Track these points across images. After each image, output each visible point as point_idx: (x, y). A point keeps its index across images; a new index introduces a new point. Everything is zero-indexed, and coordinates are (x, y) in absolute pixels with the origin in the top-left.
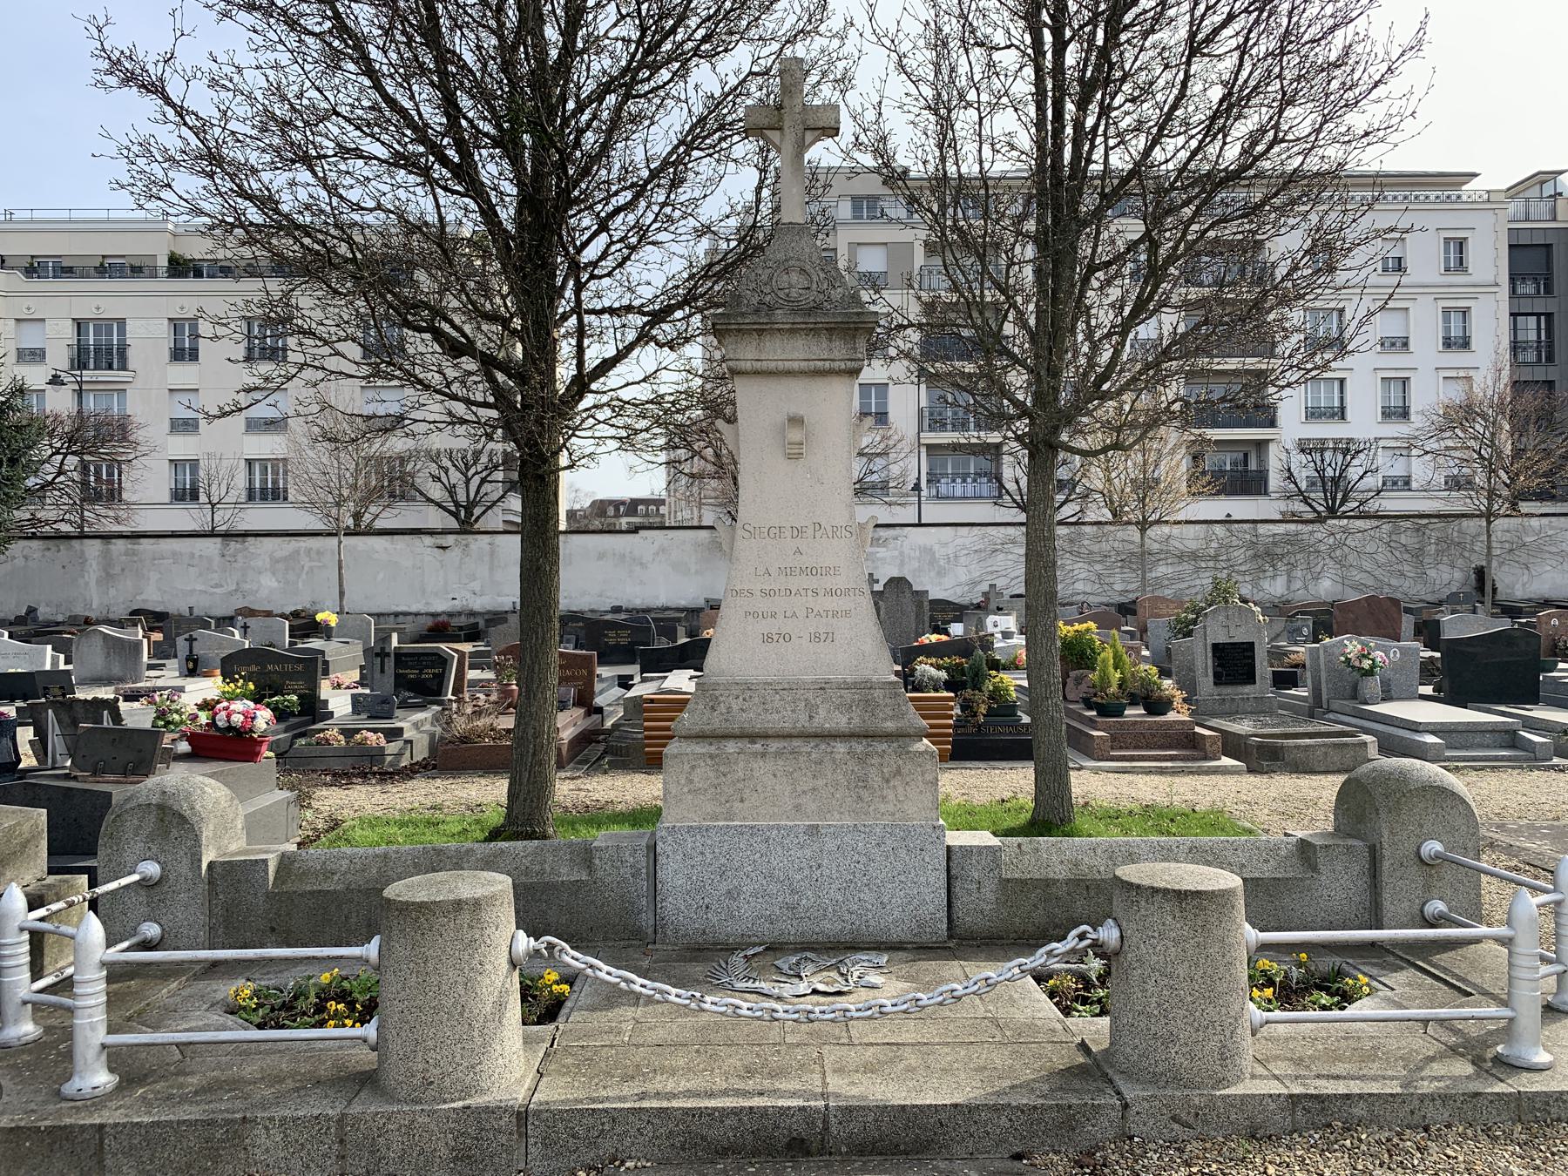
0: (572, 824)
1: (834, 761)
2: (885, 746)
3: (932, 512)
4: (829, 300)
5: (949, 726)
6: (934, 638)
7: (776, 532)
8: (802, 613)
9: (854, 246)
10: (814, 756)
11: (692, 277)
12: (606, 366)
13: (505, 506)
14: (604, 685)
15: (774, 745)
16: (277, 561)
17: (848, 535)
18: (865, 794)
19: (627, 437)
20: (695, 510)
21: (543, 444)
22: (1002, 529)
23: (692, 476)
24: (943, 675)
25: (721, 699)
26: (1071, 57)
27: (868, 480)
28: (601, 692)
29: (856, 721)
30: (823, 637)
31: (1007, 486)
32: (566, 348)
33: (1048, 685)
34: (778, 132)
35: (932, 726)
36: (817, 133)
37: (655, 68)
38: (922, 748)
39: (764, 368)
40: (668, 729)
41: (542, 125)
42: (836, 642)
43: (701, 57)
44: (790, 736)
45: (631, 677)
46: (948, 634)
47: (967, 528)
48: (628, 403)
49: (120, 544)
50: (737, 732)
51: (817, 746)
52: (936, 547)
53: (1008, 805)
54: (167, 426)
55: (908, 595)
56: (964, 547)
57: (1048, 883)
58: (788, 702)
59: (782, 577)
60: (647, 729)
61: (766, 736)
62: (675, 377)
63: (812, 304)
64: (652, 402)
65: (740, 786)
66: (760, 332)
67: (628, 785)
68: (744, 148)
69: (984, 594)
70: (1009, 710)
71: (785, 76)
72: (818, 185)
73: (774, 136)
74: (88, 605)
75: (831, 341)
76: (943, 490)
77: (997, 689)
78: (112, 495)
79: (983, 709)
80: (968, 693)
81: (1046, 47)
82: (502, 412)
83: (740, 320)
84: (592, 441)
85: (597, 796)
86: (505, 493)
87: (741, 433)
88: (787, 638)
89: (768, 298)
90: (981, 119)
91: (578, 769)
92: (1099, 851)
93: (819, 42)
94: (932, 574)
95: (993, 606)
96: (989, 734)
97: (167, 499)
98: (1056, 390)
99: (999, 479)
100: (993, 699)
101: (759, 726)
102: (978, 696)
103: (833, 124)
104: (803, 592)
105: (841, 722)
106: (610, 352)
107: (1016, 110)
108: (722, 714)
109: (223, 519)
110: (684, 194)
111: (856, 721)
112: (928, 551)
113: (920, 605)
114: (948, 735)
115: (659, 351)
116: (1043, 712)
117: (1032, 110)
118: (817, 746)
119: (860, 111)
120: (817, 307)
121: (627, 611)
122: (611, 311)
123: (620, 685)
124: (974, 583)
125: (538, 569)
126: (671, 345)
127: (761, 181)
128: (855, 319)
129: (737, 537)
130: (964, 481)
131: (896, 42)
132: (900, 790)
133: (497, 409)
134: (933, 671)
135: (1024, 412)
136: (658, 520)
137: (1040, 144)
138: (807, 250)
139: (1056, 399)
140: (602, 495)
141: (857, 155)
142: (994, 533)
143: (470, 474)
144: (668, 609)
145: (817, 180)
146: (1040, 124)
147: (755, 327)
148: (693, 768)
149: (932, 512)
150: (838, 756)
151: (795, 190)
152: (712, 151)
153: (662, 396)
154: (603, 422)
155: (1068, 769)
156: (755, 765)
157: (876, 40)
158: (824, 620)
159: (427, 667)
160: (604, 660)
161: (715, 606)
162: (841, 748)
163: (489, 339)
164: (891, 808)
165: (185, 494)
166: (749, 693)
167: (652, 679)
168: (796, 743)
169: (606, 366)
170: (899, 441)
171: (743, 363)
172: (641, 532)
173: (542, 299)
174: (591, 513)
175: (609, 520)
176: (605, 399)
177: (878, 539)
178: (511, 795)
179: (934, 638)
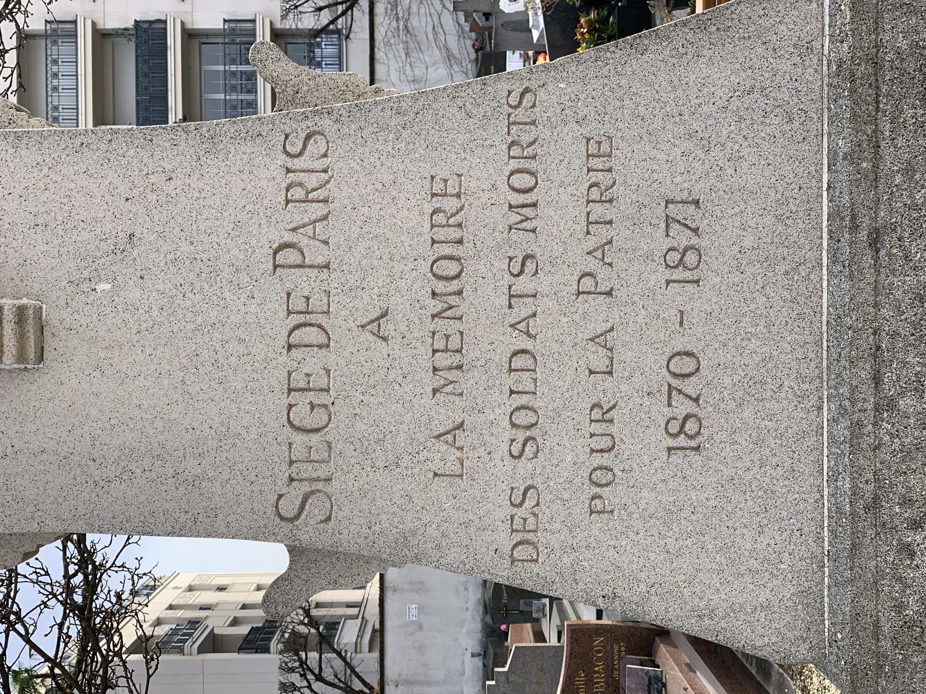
13: (351, 649)
17: (317, 146)
22: (378, 20)
30: (683, 238)
31: (325, 22)
42: (700, 189)
56: (402, 71)
59: (469, 381)
86: (335, 651)
99: (317, 33)
104: (523, 309)
142: (383, 31)
158: (620, 233)
166: (892, 509)
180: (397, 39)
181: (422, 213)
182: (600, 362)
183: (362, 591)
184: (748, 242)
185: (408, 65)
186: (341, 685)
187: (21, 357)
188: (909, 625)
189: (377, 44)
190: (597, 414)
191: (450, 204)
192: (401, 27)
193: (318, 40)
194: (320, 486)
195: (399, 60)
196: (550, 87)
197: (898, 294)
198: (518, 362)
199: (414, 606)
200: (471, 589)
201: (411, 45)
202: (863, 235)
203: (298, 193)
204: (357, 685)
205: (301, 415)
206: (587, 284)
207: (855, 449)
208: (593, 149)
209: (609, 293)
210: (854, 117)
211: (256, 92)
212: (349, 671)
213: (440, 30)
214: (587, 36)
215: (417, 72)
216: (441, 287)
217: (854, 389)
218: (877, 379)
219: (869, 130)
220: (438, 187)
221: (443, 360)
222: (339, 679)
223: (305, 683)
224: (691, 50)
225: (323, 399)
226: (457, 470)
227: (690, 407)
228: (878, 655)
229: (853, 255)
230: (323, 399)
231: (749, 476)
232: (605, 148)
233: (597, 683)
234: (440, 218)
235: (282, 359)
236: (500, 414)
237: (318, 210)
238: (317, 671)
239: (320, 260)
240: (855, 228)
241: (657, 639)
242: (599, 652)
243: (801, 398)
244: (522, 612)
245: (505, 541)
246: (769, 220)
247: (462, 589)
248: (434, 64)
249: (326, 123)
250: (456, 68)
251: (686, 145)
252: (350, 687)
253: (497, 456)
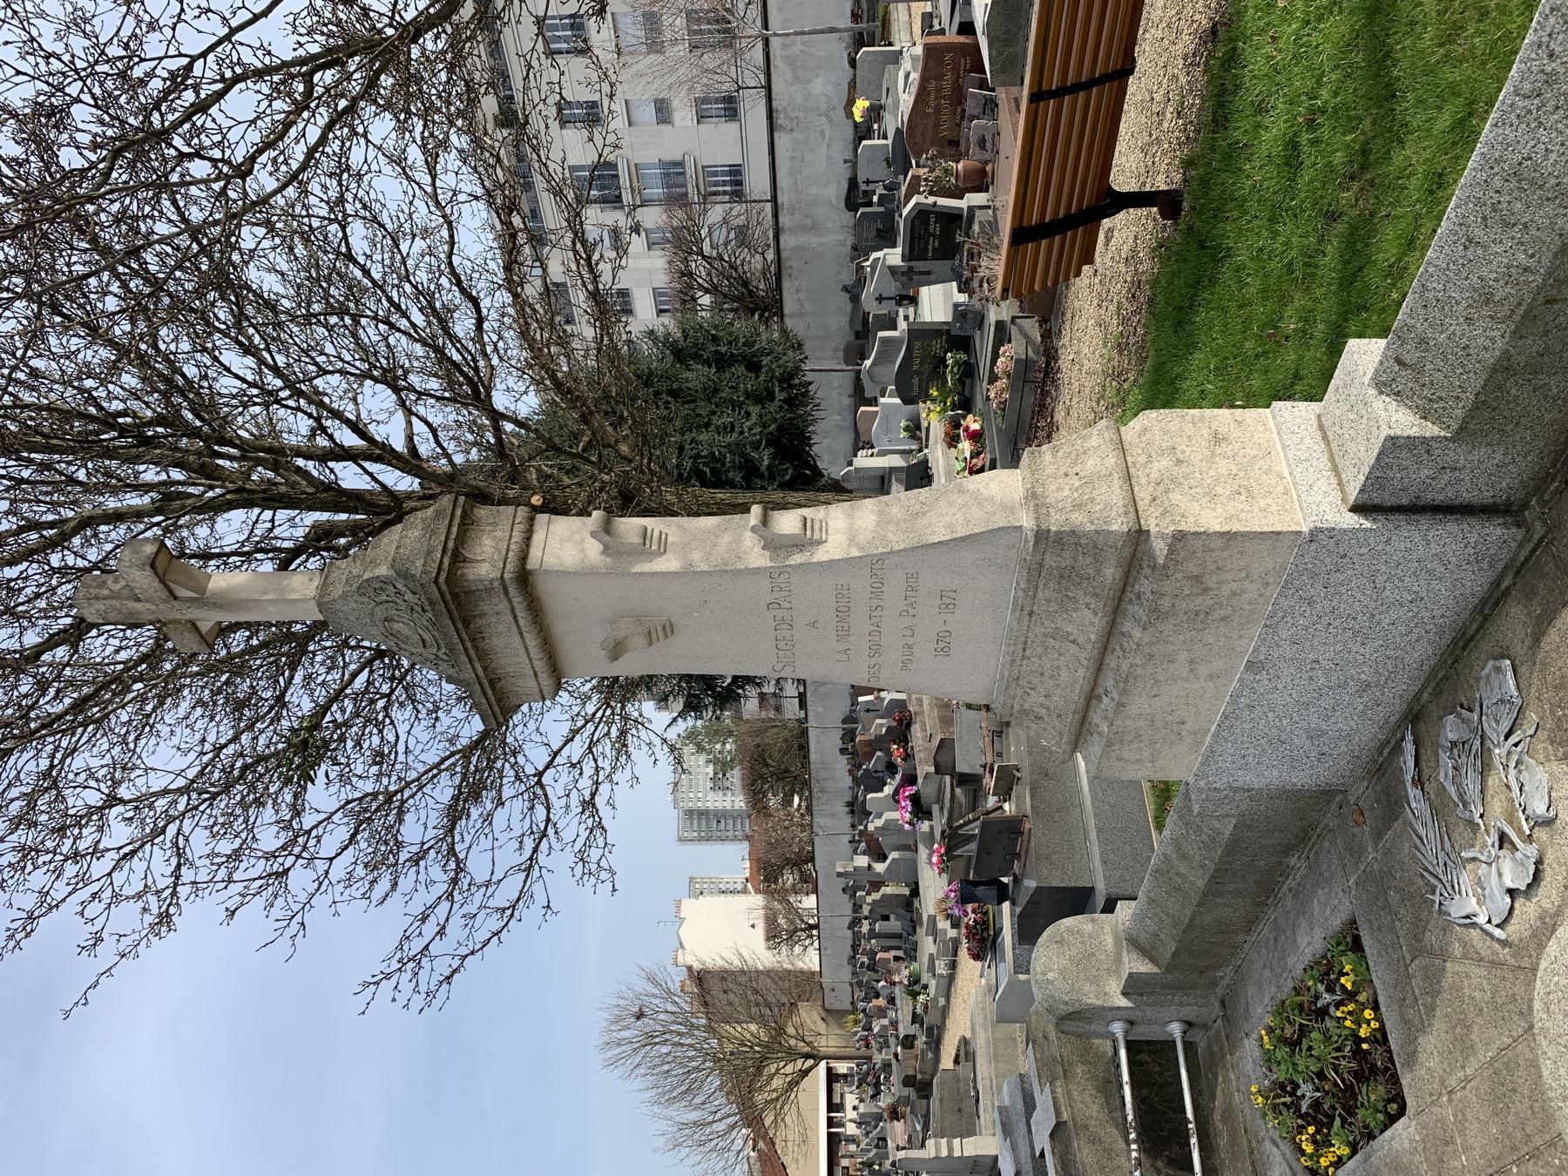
16: (797, 78)
49: (784, 220)
54: (664, 128)
57: (1503, 369)
74: (841, 243)
78: (736, 172)
92: (1478, 233)
97: (734, 126)
109: (752, 78)
147: (489, 692)
159: (927, 230)
165: (731, 108)
218: (1024, 650)
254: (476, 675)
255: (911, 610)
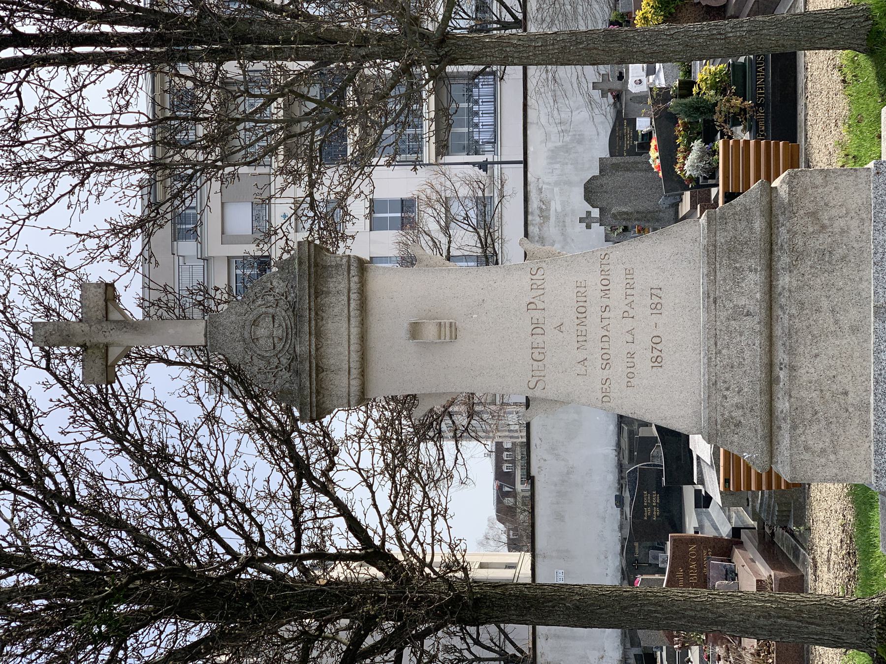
0: (869, 575)
1: (800, 288)
2: (783, 230)
3: (511, 149)
4: (285, 295)
5: (758, 145)
6: (654, 154)
7: (538, 354)
8: (629, 324)
9: (226, 238)
10: (794, 311)
11: (259, 431)
12: (355, 527)
14: (707, 524)
15: (781, 356)
17: (540, 272)
18: (839, 252)
19: (432, 508)
20: (509, 409)
21: (441, 599)
23: (470, 416)
24: (697, 145)
25: (727, 415)
26: (29, 28)
27: (474, 221)
28: (716, 529)
29: (752, 262)
30: (656, 300)
32: (339, 571)
33: (711, 37)
34: (111, 349)
35: (757, 178)
36: (111, 307)
37: (43, 472)
38: (785, 187)
39: (357, 365)
40: (759, 476)
41: (104, 598)
43: (31, 425)
44: (770, 338)
45: (698, 492)
46: (648, 136)
47: (530, 111)
48: (394, 503)
50: (765, 398)
51: (782, 307)
52: (550, 145)
53: (849, 77)
55: (604, 180)
56: (550, 115)
58: (731, 338)
60: (759, 487)
61: (770, 366)
62: (366, 455)
63: (290, 313)
64: (393, 477)
65: (828, 395)
66: (319, 369)
67: (824, 505)
68: (126, 378)
69: (604, 95)
70: (738, 74)
71: (51, 341)
72: (164, 299)
73: (114, 352)
75: (328, 293)
76: (485, 136)
77: (714, 86)
79: (737, 102)
80: (718, 118)
81: (20, 54)
82: (406, 643)
83: (307, 392)
84: (437, 547)
85: (836, 542)
87: (428, 391)
88: (656, 341)
89: (284, 361)
90: (94, 127)
91: (805, 560)
93: (14, 296)
94: (580, 149)
95: (617, 85)
96: (766, 93)
98: (382, 37)
100: (725, 90)
101: (759, 374)
102: (722, 107)
103: (101, 290)
104: (605, 322)
105: (754, 280)
106: (341, 523)
107: (84, 86)
108: (744, 415)
110: (174, 443)
111: (752, 262)
112: (554, 155)
113: (616, 167)
114: (768, 145)
115: (339, 467)
116: (742, 42)
117: (84, 68)
118: (782, 307)
119: (85, 253)
120: (293, 307)
121: (621, 488)
122: (297, 523)
123: (707, 506)
124: (591, 102)
125: (577, 608)
126: (332, 454)
127: (161, 360)
128: (305, 267)
129: (543, 396)
130: (476, 114)
131: (15, 219)
132: (834, 212)
133: (403, 649)
134: (693, 156)
135: (405, 70)
136: (518, 449)
137: (118, 61)
138: (233, 318)
139: (391, 36)
140: (492, 512)
141: (132, 256)
142: (534, 81)
143: (470, 657)
144: (618, 445)
145: (160, 300)
146: (96, 60)
148: (807, 448)
149: (511, 149)
150: (795, 284)
151: (171, 331)
152: (128, 410)
153: (387, 465)
154: (416, 531)
155: (806, 14)
156: (805, 378)
157: (12, 241)
160: (677, 525)
161: (622, 420)
162: (784, 281)
163: (327, 649)
164: (854, 223)
166: (720, 384)
167: (700, 472)
168: (778, 331)
169: (355, 527)
170: (432, 187)
171: (353, 389)
172: (532, 474)
173: (285, 596)
174: (511, 522)
175: (519, 504)
176: (391, 531)
177: (541, 209)
178: (835, 643)
179: (654, 154)
180: (546, 88)
181: (573, 292)
182: (630, 339)
183: (513, 571)
184: (677, 301)
185: (556, 110)
186: (497, 649)
187: (451, 338)
188: (725, 420)
189: (529, 93)
190: (629, 355)
191: (582, 290)
192: (550, 78)
193: (476, 80)
194: (542, 378)
195: (548, 105)
196: (614, 253)
197: (722, 318)
198: (604, 339)
199: (561, 571)
200: (610, 558)
201: (558, 93)
202: (712, 299)
203: (535, 286)
204: (511, 650)
205: (536, 356)
206: (626, 315)
207: (709, 366)
208: (627, 272)
209: (633, 317)
210: (708, 263)
211: (422, 127)
212: (503, 637)
213: (583, 80)
214: (682, 133)
215: (563, 115)
216: (580, 316)
217: (709, 347)
218: (716, 344)
219: (713, 267)
220: (579, 284)
221: (580, 339)
222: (495, 644)
223: (465, 646)
224: (658, 241)
225: (543, 351)
226: (585, 373)
227: (659, 353)
228: (717, 430)
229: (708, 305)
230: (543, 351)
231: (677, 375)
232: (631, 272)
233: (691, 576)
234: (579, 294)
235: (530, 338)
236: (599, 356)
237: (541, 292)
238: (475, 636)
239: (542, 308)
240: (709, 297)
241: (734, 547)
242: (692, 555)
243: (694, 350)
244: (650, 565)
245: (600, 396)
246: (683, 294)
247: (602, 557)
248: (577, 109)
249: (544, 265)
250: (596, 111)
251: (657, 271)
252: (504, 651)
253: (597, 369)
254: (310, 352)
255: (630, 311)
